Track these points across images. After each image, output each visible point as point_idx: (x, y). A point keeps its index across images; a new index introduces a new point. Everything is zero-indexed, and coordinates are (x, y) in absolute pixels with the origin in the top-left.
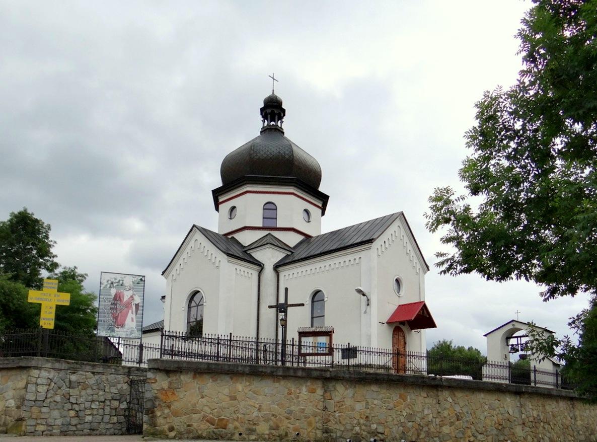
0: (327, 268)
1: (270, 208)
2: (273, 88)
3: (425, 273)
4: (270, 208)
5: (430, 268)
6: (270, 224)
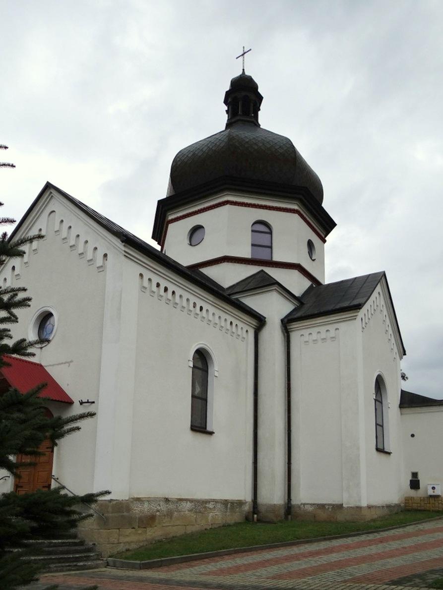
0: (323, 335)
1: (263, 228)
2: (243, 66)
3: (401, 358)
4: (263, 228)
5: (407, 353)
6: (263, 255)
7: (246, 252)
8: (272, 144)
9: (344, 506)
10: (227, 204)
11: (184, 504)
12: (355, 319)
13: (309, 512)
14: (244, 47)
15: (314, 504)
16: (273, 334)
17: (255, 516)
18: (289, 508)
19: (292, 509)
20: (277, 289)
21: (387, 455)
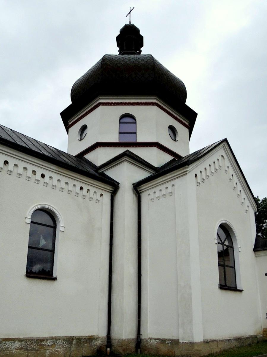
0: (163, 192)
1: (127, 119)
2: (130, 20)
4: (127, 119)
7: (114, 138)
8: (136, 59)
9: (180, 341)
10: (100, 106)
11: (11, 344)
12: (186, 174)
13: (154, 347)
14: (130, 8)
15: (158, 339)
16: (126, 196)
17: (108, 349)
18: (139, 341)
19: (142, 344)
20: (127, 159)
21: (238, 293)
